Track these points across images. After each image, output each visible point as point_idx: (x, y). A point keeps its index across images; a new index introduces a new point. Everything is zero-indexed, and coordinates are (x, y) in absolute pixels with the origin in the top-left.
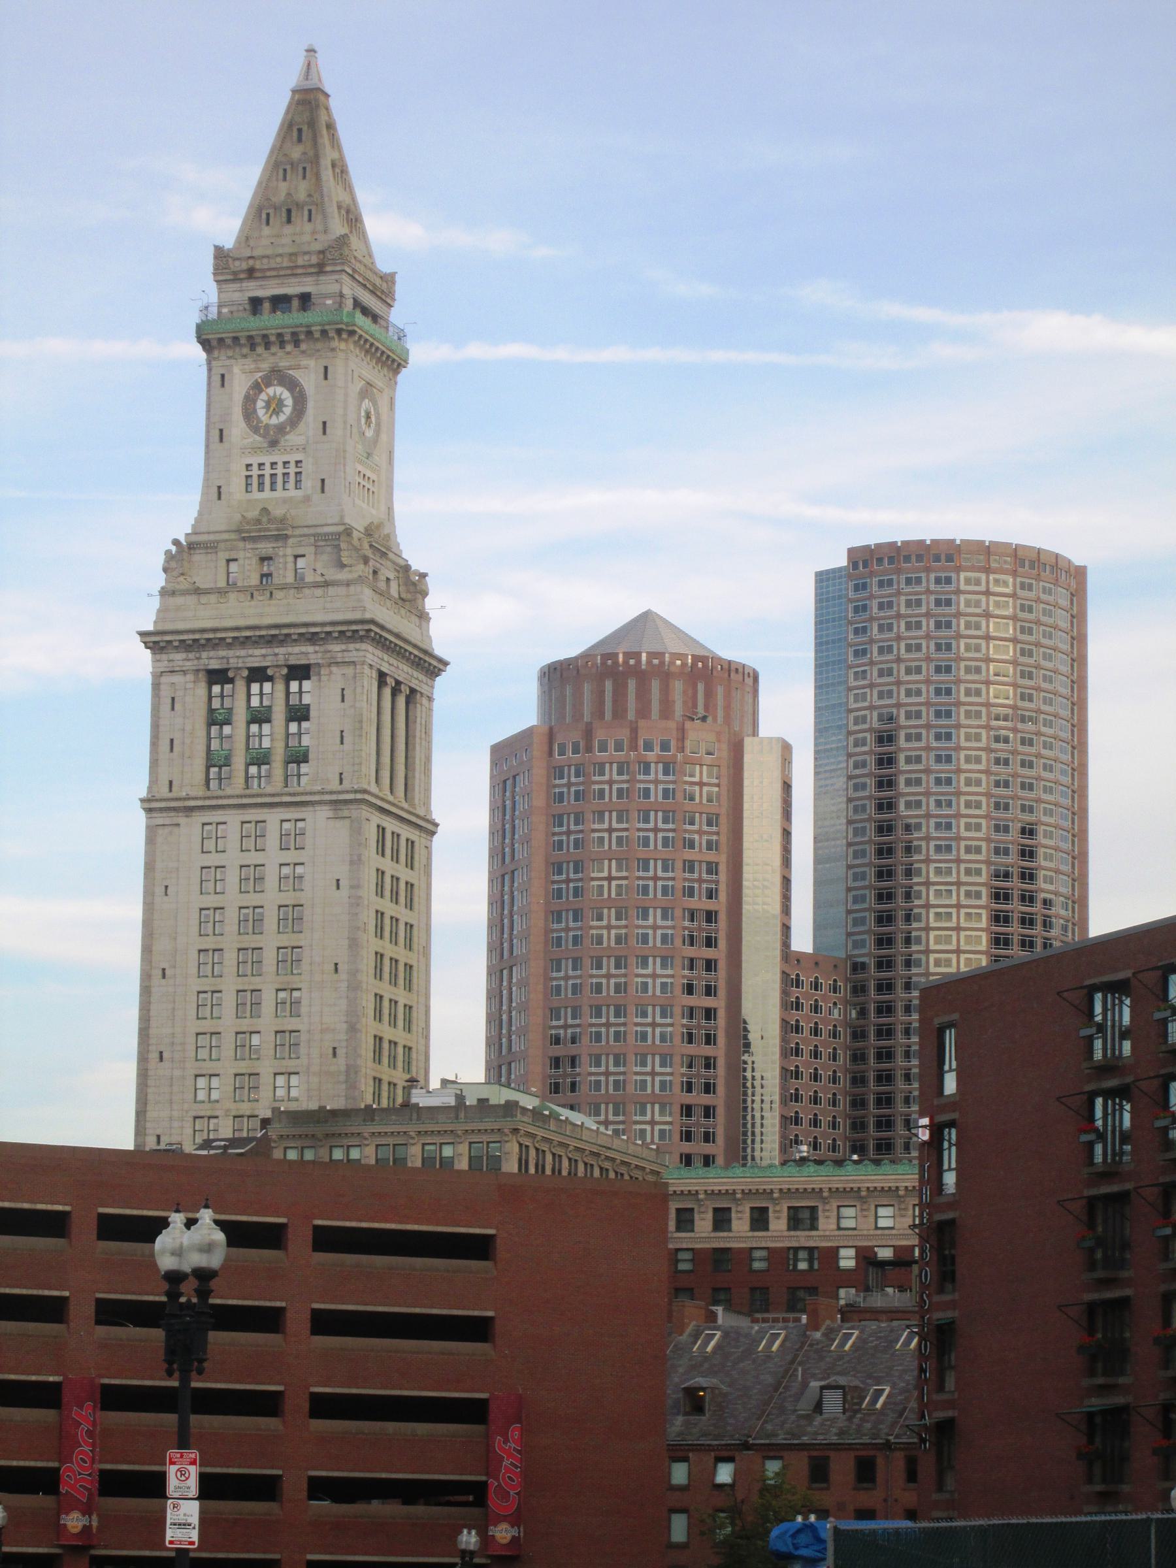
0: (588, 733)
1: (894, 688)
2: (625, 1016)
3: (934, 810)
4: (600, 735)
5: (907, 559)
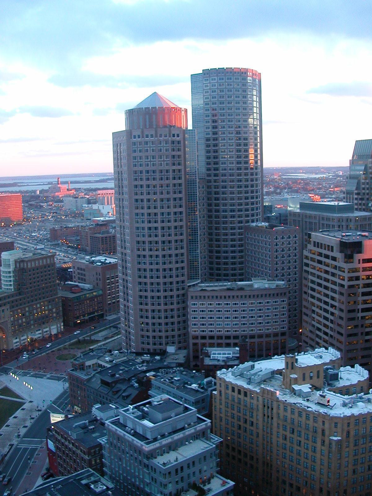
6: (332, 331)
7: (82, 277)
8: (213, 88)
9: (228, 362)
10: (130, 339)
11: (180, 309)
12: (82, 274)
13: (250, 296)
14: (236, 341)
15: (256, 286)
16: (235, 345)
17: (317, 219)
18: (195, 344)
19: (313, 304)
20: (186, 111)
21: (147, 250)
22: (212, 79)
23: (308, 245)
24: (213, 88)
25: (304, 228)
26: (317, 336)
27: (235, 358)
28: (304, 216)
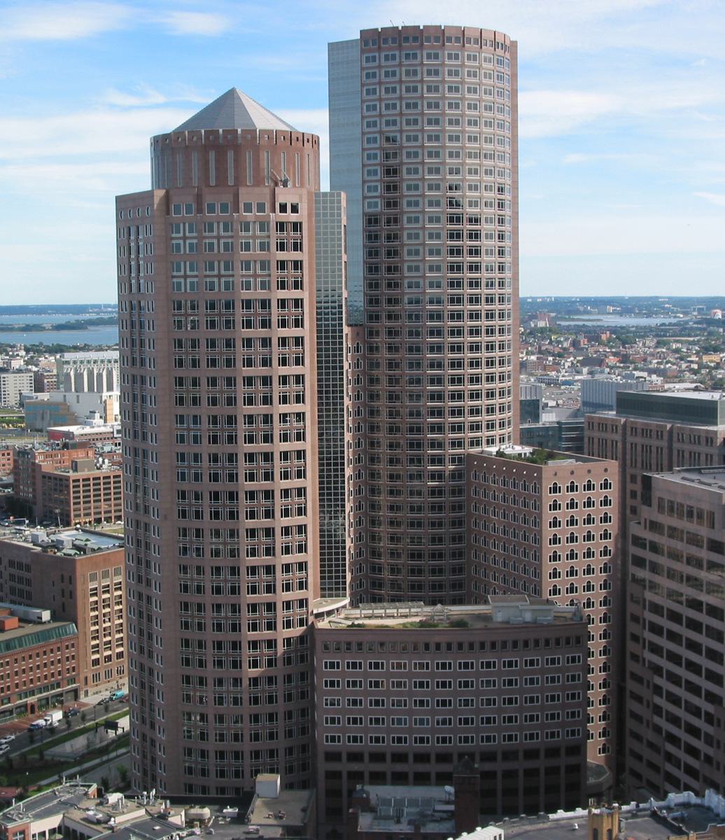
0: (199, 198)
1: (377, 71)
2: (233, 270)
3: (384, 95)
4: (208, 199)
5: (406, 39)
6: (711, 745)
7: (21, 586)
8: (388, 80)
9: (424, 825)
10: (153, 760)
11: (294, 677)
12: (20, 580)
13: (482, 645)
14: (445, 768)
15: (499, 617)
16: (443, 779)
17: (620, 431)
18: (333, 775)
19: (657, 670)
20: (315, 141)
21: (207, 516)
22: (387, 58)
23: (645, 508)
24: (388, 80)
25: (628, 462)
26: (669, 757)
27: (445, 815)
28: (629, 429)
